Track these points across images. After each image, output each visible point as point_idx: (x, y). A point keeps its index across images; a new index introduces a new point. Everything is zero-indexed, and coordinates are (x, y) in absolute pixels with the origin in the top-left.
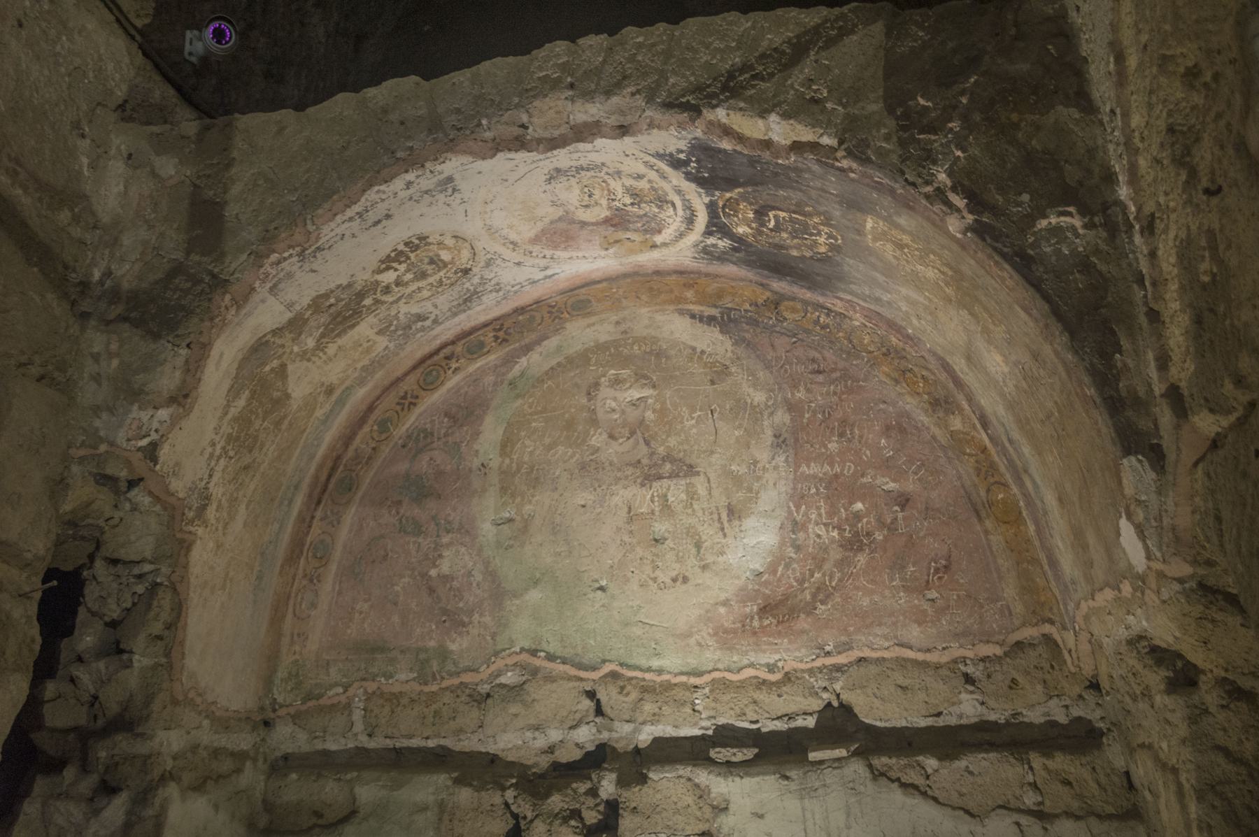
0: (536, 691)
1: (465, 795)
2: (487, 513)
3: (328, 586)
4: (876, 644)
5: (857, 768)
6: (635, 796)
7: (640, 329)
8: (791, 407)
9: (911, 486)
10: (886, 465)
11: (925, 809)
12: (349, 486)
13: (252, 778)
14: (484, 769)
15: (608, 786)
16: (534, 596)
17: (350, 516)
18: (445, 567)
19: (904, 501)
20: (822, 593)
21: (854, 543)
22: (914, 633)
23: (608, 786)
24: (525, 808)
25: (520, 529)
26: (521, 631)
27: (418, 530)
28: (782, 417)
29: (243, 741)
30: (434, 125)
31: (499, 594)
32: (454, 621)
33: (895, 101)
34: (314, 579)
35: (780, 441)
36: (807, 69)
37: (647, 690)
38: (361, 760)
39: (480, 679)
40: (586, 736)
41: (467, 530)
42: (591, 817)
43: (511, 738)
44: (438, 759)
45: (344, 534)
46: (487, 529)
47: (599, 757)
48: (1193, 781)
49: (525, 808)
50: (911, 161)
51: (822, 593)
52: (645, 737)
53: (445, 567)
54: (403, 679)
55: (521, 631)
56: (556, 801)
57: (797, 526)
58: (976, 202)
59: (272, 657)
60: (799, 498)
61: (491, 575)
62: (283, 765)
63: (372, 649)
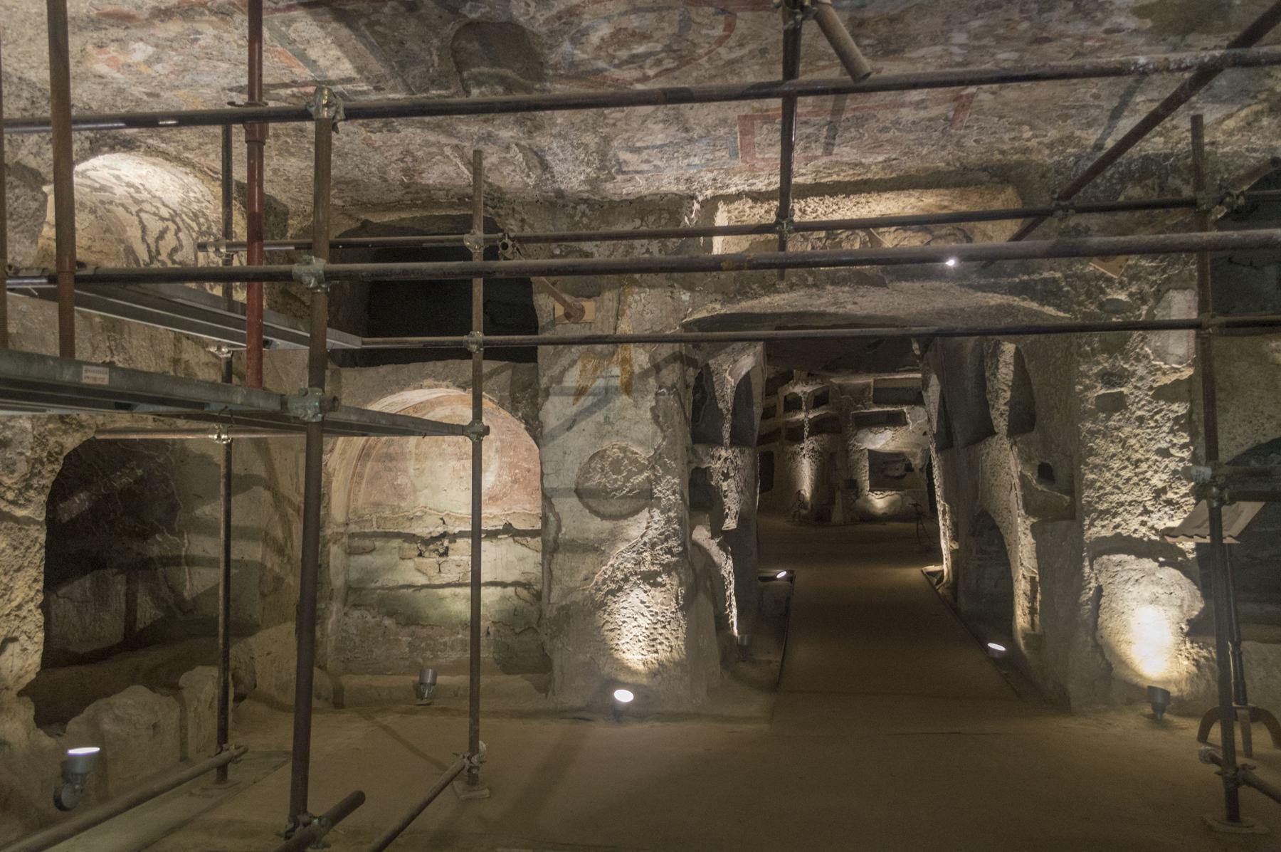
0: (427, 518)
1: (406, 545)
2: (411, 466)
3: (363, 486)
4: (518, 508)
5: (511, 540)
6: (452, 546)
7: (458, 413)
8: (501, 441)
9: (531, 466)
10: (525, 460)
11: (526, 550)
12: (368, 455)
13: (345, 539)
14: (411, 538)
15: (446, 543)
16: (426, 491)
17: (369, 465)
18: (399, 482)
19: (529, 471)
20: (505, 495)
21: (515, 481)
22: (528, 506)
23: (446, 543)
24: (423, 548)
25: (422, 472)
26: (422, 501)
27: (390, 470)
28: (498, 443)
29: (342, 530)
30: (398, 384)
31: (415, 491)
32: (402, 497)
33: (512, 394)
34: (359, 483)
35: (497, 451)
36: (492, 381)
37: (457, 518)
38: (375, 535)
39: (410, 514)
40: (441, 530)
41: (405, 471)
42: (441, 551)
43: (419, 530)
44: (398, 535)
45: (367, 470)
46: (411, 471)
47: (444, 535)
48: (411, 572)
49: (423, 548)
50: (514, 411)
51: (505, 495)
52: (456, 531)
53: (399, 482)
54: (387, 513)
55: (422, 501)
56: (431, 547)
57: (500, 476)
58: (527, 423)
59: (348, 507)
60: (501, 468)
61: (413, 485)
62: (352, 536)
63: (378, 505)
